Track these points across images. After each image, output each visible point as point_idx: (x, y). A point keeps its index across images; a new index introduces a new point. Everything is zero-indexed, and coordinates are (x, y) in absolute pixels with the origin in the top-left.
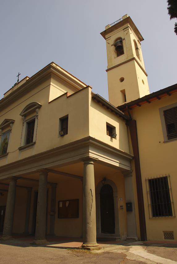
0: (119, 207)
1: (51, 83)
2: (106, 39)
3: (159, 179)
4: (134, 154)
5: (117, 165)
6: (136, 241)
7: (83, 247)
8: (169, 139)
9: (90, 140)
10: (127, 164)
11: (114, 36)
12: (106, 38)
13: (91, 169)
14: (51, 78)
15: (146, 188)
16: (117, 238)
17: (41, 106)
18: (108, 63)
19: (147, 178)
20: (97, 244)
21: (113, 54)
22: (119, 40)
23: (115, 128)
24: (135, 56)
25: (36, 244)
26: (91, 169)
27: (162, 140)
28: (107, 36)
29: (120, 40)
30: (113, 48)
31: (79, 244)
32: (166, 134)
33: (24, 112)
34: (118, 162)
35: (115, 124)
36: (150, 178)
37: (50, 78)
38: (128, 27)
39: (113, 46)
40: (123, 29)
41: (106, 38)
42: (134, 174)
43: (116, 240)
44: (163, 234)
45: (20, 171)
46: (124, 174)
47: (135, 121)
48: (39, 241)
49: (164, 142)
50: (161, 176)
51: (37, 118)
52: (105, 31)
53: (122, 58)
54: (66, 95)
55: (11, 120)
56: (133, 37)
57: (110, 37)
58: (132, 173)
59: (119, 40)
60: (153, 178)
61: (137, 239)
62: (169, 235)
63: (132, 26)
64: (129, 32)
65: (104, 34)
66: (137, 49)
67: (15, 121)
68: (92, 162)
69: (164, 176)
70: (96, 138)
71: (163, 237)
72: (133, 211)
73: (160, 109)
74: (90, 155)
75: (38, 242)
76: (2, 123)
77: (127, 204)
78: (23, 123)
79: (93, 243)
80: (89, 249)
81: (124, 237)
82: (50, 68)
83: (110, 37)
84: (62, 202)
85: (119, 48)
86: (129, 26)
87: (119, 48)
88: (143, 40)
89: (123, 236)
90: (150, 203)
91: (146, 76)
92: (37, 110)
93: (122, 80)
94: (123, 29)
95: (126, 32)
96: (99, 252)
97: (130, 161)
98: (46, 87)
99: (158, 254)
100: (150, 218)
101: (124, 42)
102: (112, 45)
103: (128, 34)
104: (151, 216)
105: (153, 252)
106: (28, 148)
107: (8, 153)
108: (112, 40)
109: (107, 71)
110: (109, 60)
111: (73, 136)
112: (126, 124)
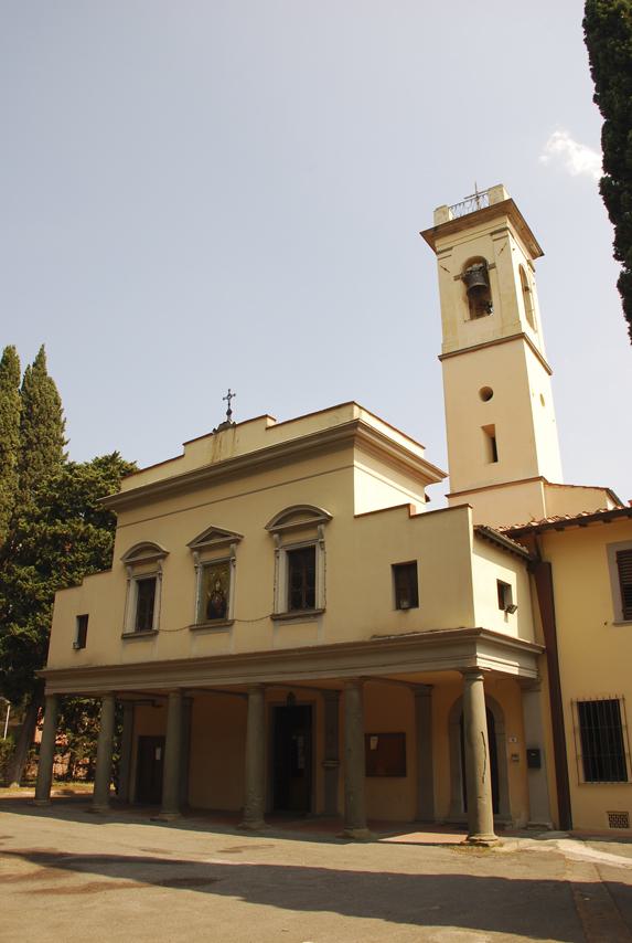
0: (508, 756)
1: (355, 463)
2: (437, 253)
3: (601, 702)
4: (546, 644)
5: (515, 671)
6: (549, 830)
7: (473, 843)
8: (626, 618)
9: (482, 635)
10: (531, 664)
11: (466, 247)
12: (438, 249)
13: (479, 688)
14: (355, 450)
15: (571, 720)
16: (507, 823)
17: (331, 518)
18: (445, 332)
19: (575, 700)
20: (496, 837)
21: (461, 309)
22: (476, 266)
23: (510, 586)
24: (525, 328)
25: (353, 838)
26: (479, 688)
27: (612, 620)
28: (441, 244)
29: (481, 265)
30: (459, 288)
31: (461, 838)
32: (621, 608)
33: (276, 524)
34: (517, 664)
35: (511, 576)
36: (581, 700)
37: (352, 447)
38: (507, 229)
39: (460, 285)
40: (492, 234)
41: (438, 249)
42: (545, 687)
43: (507, 828)
44: (606, 817)
45: (284, 673)
46: (522, 685)
47: (550, 565)
48: (358, 831)
49: (615, 624)
50: (607, 698)
51: (323, 549)
52: (436, 228)
53: (485, 328)
54: (406, 509)
55: (235, 534)
56: (518, 255)
57: (451, 249)
58: (539, 683)
59: (476, 266)
60: (587, 699)
61: (551, 827)
62: (618, 819)
63: (515, 224)
64: (507, 244)
65: (431, 236)
66: (526, 289)
67: (242, 537)
68: (481, 677)
69: (614, 698)
70: (491, 629)
71: (608, 823)
72: (543, 769)
73: (609, 546)
74: (478, 664)
75: (355, 833)
76: (197, 538)
77: (529, 752)
78: (277, 551)
79: (489, 835)
80: (487, 845)
81: (520, 821)
82: (356, 427)
83: (451, 249)
84: (376, 738)
85: (478, 291)
86: (509, 225)
87: (478, 291)
88: (542, 254)
89: (517, 821)
90: (579, 752)
91: (547, 374)
92: (322, 526)
93: (487, 395)
94: (492, 234)
95: (500, 244)
96: (504, 849)
97: (535, 657)
98: (343, 468)
99: (614, 853)
100: (579, 784)
101: (492, 273)
102: (456, 278)
103: (505, 249)
104: (582, 781)
105: (605, 850)
106: (301, 620)
107: (233, 621)
108: (456, 265)
109: (442, 358)
110: (448, 327)
111: (429, 617)
112: (528, 570)
